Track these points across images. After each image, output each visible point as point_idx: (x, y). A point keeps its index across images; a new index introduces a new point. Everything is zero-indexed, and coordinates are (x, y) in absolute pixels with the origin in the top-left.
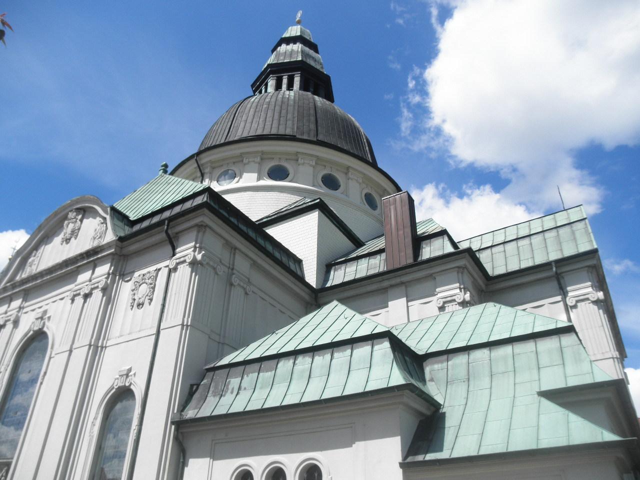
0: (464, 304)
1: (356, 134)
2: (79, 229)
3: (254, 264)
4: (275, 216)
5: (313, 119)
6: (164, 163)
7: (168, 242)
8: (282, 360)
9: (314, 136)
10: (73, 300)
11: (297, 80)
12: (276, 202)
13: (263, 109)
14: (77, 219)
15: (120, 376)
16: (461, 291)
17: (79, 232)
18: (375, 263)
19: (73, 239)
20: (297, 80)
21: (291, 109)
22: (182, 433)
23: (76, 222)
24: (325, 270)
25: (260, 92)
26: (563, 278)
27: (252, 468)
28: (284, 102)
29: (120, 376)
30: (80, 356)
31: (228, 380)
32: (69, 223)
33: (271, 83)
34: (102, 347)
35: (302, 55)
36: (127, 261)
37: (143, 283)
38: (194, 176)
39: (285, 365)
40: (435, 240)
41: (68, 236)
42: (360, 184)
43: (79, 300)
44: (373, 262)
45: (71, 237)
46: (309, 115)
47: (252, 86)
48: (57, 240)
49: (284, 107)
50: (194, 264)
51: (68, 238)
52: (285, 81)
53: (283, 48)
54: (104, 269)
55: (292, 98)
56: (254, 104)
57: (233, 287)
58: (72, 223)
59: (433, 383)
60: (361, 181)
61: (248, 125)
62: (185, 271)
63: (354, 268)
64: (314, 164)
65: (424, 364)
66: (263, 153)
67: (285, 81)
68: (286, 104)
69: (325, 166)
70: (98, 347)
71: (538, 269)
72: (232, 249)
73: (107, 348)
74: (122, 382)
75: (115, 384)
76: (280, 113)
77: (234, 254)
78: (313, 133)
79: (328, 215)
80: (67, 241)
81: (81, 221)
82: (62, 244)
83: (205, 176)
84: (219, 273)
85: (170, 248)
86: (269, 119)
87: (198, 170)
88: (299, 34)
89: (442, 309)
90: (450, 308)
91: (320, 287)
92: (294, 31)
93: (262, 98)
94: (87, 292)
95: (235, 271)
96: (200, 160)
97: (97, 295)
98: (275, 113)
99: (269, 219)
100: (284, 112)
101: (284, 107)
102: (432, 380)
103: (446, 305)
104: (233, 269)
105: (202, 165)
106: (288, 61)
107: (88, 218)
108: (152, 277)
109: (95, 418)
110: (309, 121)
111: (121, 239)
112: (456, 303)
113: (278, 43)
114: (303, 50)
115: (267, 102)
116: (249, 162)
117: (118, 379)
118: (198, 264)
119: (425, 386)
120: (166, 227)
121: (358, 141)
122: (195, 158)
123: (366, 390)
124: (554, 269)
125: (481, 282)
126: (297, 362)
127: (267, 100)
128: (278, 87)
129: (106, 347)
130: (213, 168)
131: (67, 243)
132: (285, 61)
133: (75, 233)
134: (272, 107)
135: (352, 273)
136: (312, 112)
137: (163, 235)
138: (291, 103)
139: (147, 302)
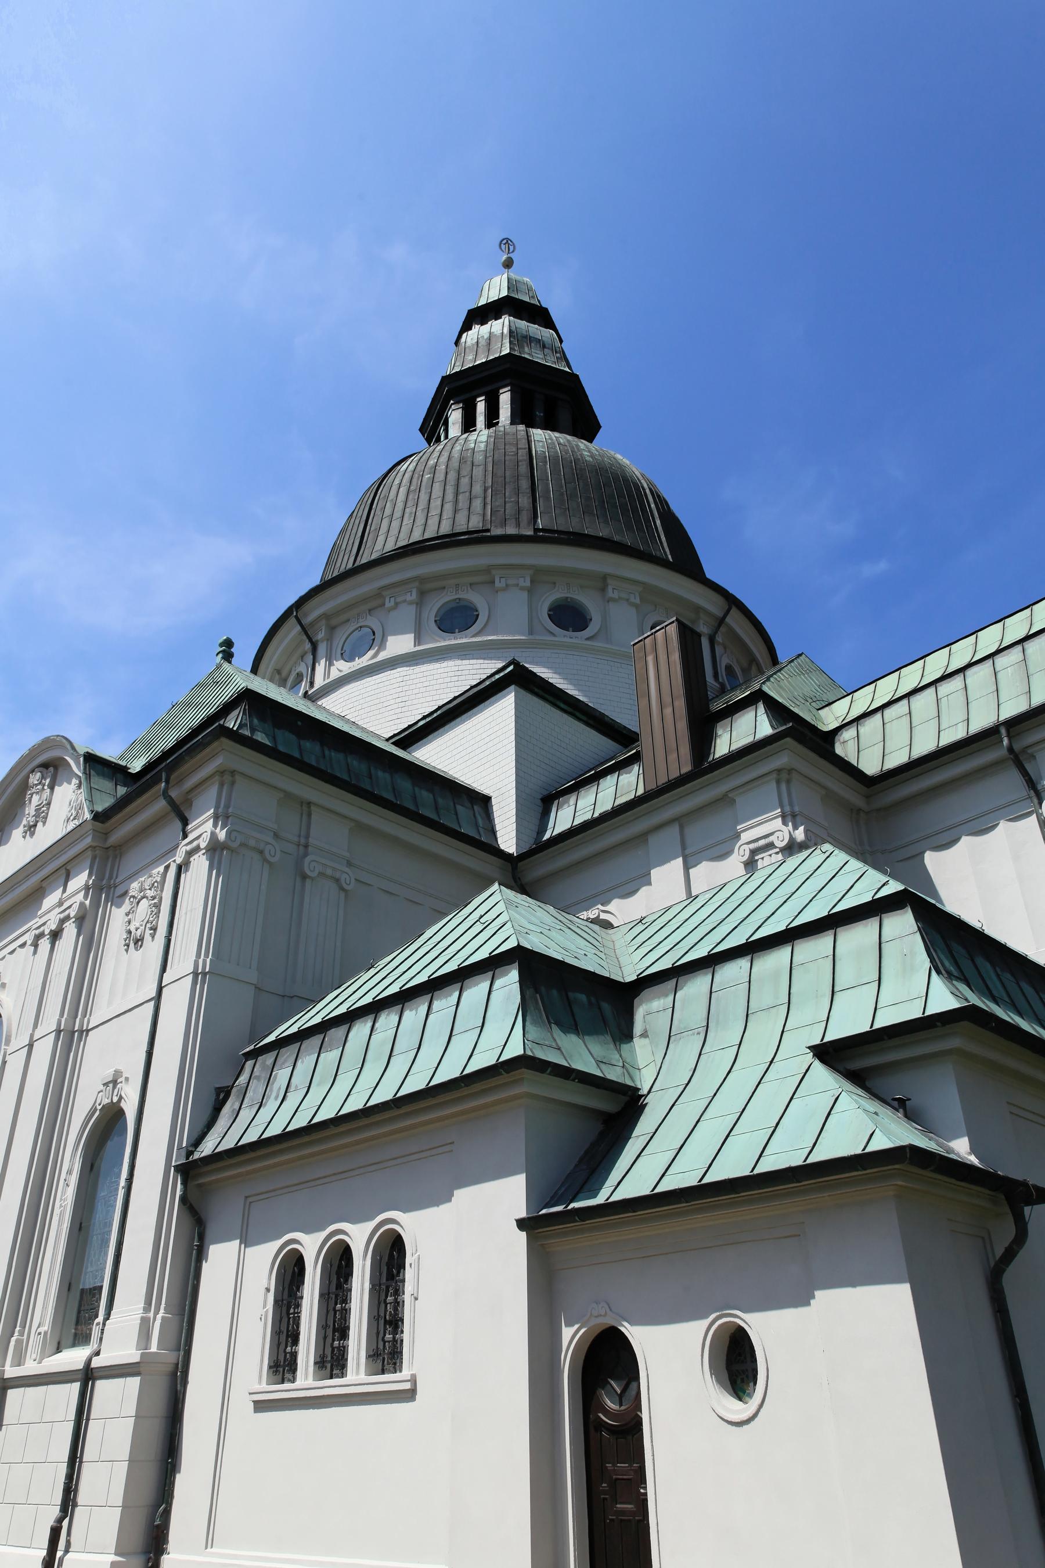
0: (791, 848)
1: (630, 496)
2: (49, 804)
3: (359, 828)
4: (439, 712)
5: (525, 484)
6: (225, 638)
7: (173, 815)
8: (356, 1024)
9: (529, 523)
10: (35, 945)
11: (505, 398)
12: (456, 678)
13: (424, 483)
14: (44, 785)
15: (104, 1085)
16: (785, 823)
17: (48, 809)
18: (629, 782)
19: (40, 824)
20: (505, 398)
21: (478, 472)
22: (200, 1186)
23: (43, 789)
24: (540, 810)
25: (438, 440)
26: (1033, 757)
27: (350, 1237)
28: (466, 459)
29: (104, 1085)
30: (44, 1050)
31: (274, 1073)
32: (32, 795)
33: (455, 416)
34: (81, 1032)
35: (511, 342)
36: (121, 856)
37: (143, 898)
38: (299, 652)
39: (360, 1030)
40: (740, 717)
41: (32, 820)
42: (636, 606)
43: (45, 944)
44: (626, 781)
45: (37, 822)
46: (517, 478)
47: (422, 430)
48: (17, 833)
49: (465, 471)
50: (214, 849)
51: (32, 823)
52: (481, 407)
53: (479, 332)
54: (80, 880)
55: (482, 446)
56: (407, 476)
57: (308, 882)
58: (37, 793)
59: (647, 1040)
60: (638, 601)
61: (395, 524)
62: (200, 864)
63: (591, 798)
64: (528, 584)
65: (636, 1001)
66: (421, 580)
67: (481, 407)
68: (469, 463)
69: (555, 583)
70: (74, 1032)
71: (975, 746)
72: (302, 806)
73: (90, 1033)
74: (107, 1096)
75: (98, 1102)
76: (457, 485)
77: (309, 815)
78: (525, 517)
79: (541, 693)
80: (31, 829)
81: (52, 788)
82: (24, 837)
83: (322, 649)
84: (272, 860)
85: (178, 825)
86: (436, 503)
87: (305, 637)
88: (504, 293)
89: (750, 865)
90: (766, 861)
91: (527, 846)
92: (496, 289)
93: (422, 459)
94: (53, 927)
95: (310, 849)
96: (306, 615)
97: (70, 930)
98: (447, 487)
99: (428, 720)
100: (465, 481)
101: (465, 471)
102: (644, 1035)
103: (756, 858)
104: (306, 846)
105: (312, 624)
106: (484, 360)
107: (60, 785)
108: (156, 884)
109: (70, 1172)
110: (517, 491)
111: (98, 817)
112: (778, 850)
113: (464, 323)
114: (513, 329)
115: (431, 468)
116: (397, 604)
117: (102, 1091)
118: (223, 849)
119: (625, 1047)
120: (163, 784)
121: (635, 510)
122: (295, 614)
123: (876, 1026)
124: (1006, 742)
125: (851, 794)
126: (377, 1025)
127: (432, 462)
128: (469, 424)
129: (88, 1031)
130: (332, 629)
131: (32, 834)
132: (478, 363)
133: (42, 815)
134: (440, 476)
135: (588, 809)
136: (524, 468)
137: (161, 804)
138: (479, 458)
139: (148, 932)
